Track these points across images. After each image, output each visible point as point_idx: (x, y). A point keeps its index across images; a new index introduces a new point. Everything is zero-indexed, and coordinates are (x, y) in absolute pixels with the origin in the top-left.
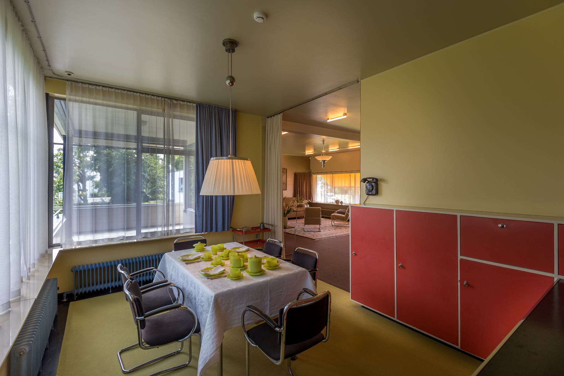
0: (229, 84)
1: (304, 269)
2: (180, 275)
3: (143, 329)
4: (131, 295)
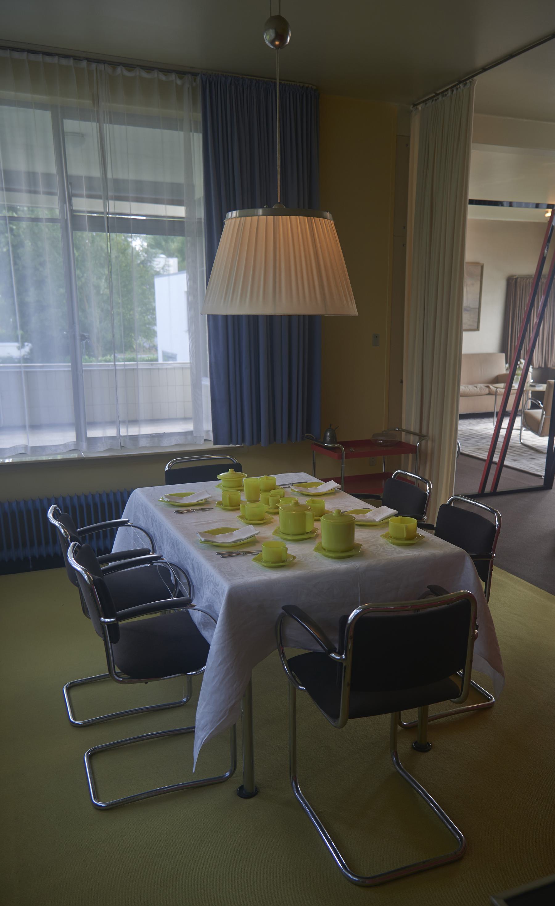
0: (272, 42)
1: (458, 549)
2: (165, 537)
3: (115, 643)
4: (85, 571)
